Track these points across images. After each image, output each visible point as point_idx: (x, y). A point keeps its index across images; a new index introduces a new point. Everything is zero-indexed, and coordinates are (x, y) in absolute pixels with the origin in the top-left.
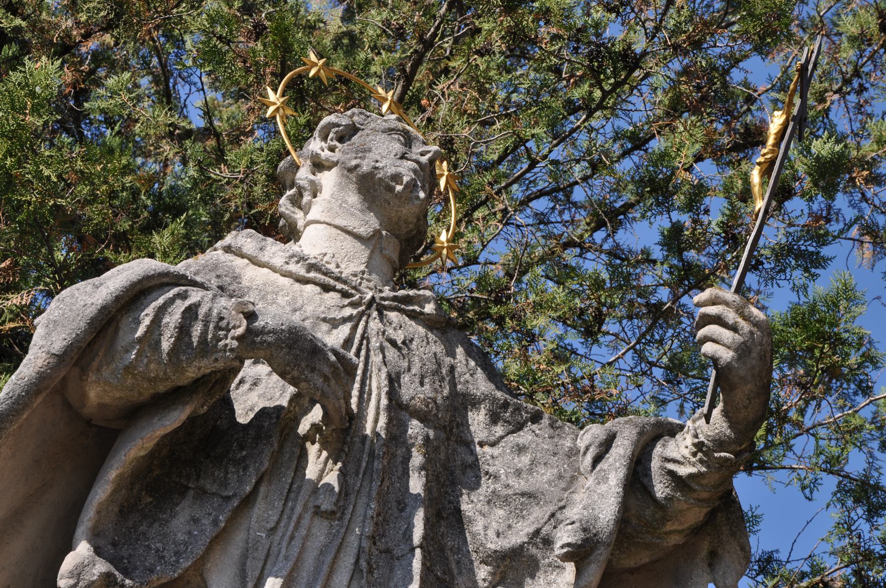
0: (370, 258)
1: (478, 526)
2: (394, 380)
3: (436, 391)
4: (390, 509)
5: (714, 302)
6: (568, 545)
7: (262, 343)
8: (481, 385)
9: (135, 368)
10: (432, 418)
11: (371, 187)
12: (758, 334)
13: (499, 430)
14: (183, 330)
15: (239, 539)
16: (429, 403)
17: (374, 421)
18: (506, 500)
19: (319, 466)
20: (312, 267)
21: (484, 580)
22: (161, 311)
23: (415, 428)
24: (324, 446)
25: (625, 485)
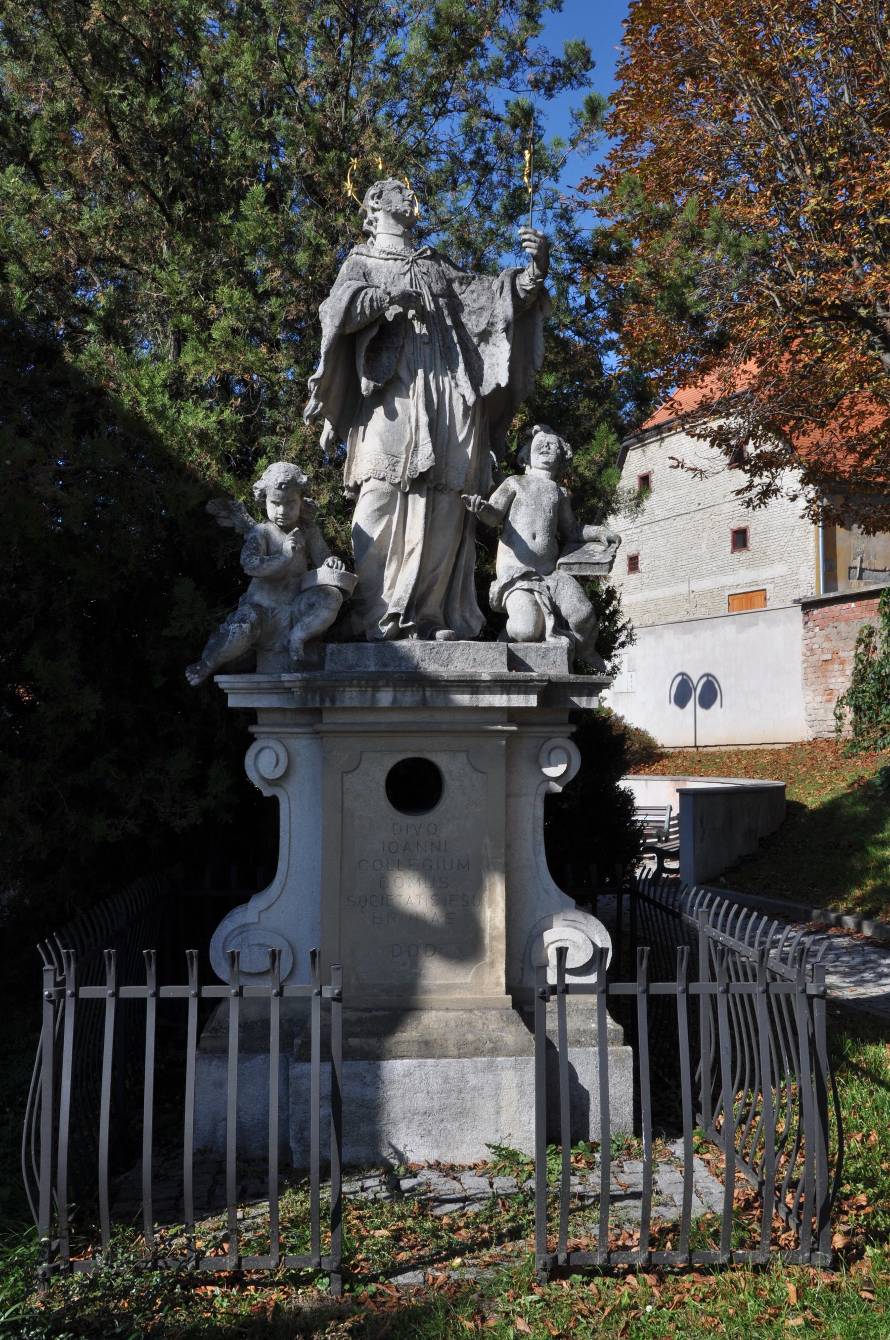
1: (470, 326)
2: (430, 288)
5: (525, 233)
8: (454, 273)
11: (397, 217)
13: (464, 287)
14: (371, 306)
15: (404, 358)
17: (430, 306)
18: (474, 312)
19: (420, 328)
20: (388, 254)
22: (362, 302)
23: (441, 301)
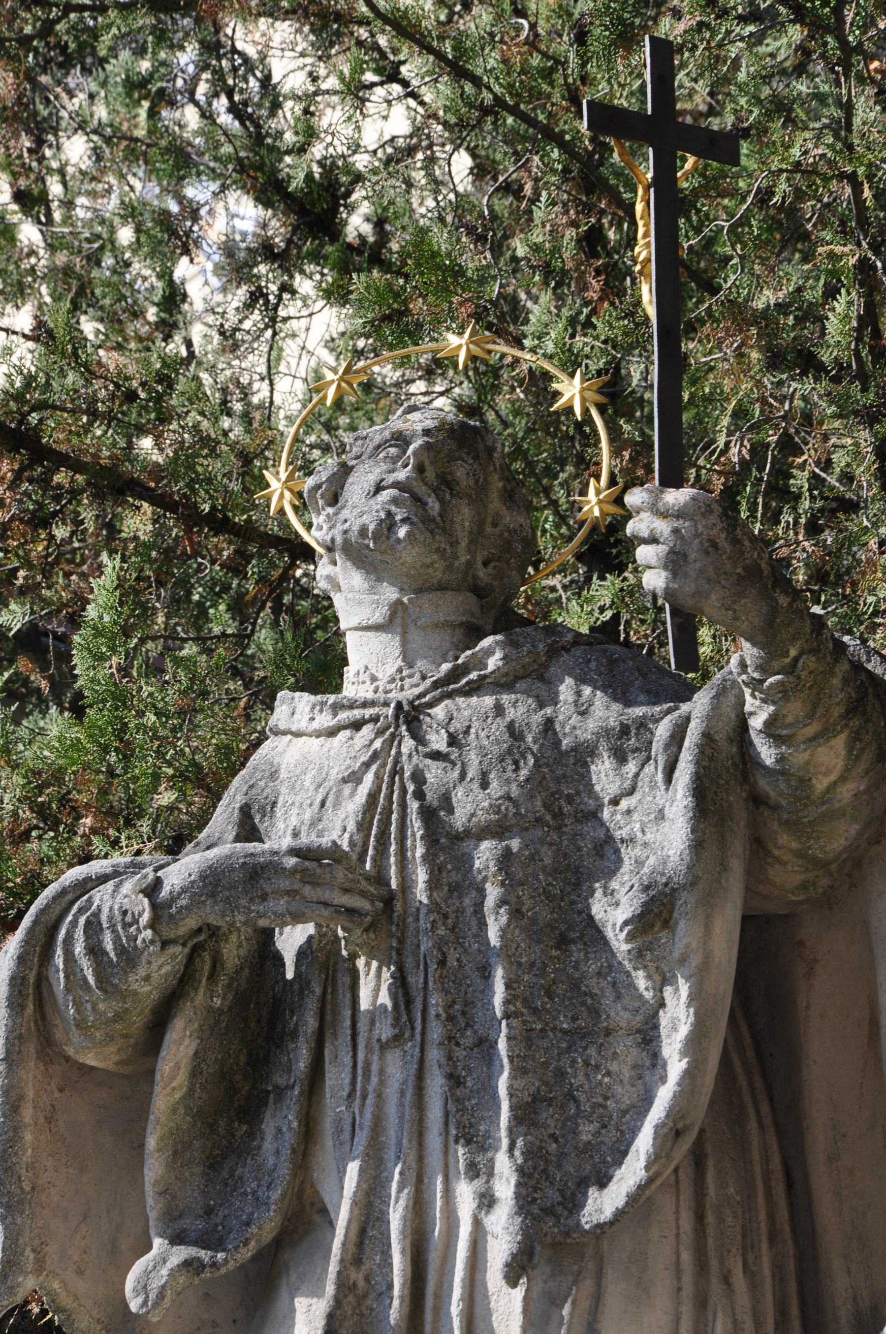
0: (404, 643)
3: (508, 781)
4: (469, 986)
6: (626, 923)
7: (179, 912)
9: (84, 1020)
10: (513, 822)
12: (685, 525)
13: (631, 767)
14: (95, 950)
16: (499, 806)
21: (647, 989)
24: (370, 956)
25: (694, 789)
